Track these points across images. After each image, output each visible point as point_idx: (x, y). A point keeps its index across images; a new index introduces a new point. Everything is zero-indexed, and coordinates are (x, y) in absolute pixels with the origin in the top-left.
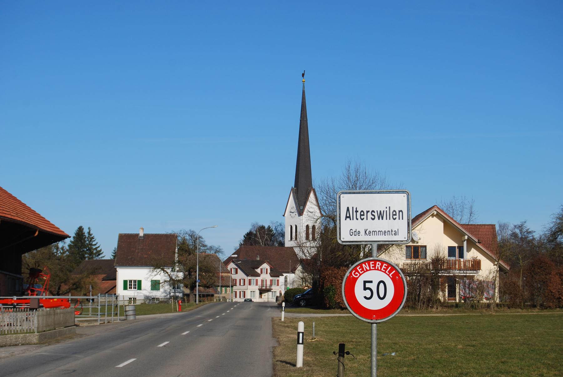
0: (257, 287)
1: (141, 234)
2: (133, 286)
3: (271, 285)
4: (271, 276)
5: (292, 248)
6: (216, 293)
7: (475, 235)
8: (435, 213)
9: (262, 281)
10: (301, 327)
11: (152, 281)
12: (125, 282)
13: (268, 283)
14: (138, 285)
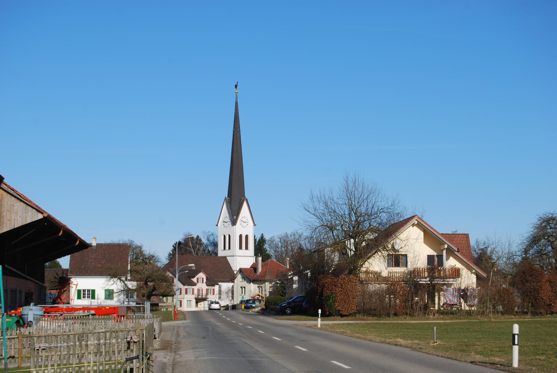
0: (194, 296)
1: (94, 244)
2: (86, 296)
3: (207, 294)
4: (207, 285)
5: (225, 258)
6: (161, 302)
7: (455, 244)
8: (416, 222)
9: (198, 290)
10: (516, 329)
11: (106, 290)
12: (79, 291)
13: (204, 292)
14: (92, 294)
